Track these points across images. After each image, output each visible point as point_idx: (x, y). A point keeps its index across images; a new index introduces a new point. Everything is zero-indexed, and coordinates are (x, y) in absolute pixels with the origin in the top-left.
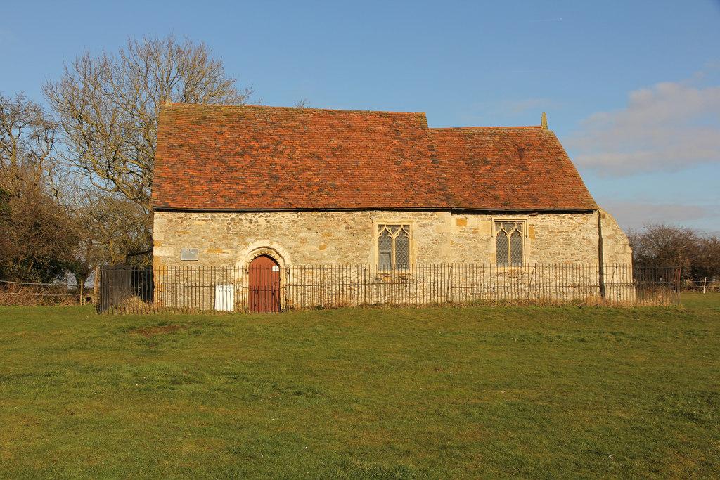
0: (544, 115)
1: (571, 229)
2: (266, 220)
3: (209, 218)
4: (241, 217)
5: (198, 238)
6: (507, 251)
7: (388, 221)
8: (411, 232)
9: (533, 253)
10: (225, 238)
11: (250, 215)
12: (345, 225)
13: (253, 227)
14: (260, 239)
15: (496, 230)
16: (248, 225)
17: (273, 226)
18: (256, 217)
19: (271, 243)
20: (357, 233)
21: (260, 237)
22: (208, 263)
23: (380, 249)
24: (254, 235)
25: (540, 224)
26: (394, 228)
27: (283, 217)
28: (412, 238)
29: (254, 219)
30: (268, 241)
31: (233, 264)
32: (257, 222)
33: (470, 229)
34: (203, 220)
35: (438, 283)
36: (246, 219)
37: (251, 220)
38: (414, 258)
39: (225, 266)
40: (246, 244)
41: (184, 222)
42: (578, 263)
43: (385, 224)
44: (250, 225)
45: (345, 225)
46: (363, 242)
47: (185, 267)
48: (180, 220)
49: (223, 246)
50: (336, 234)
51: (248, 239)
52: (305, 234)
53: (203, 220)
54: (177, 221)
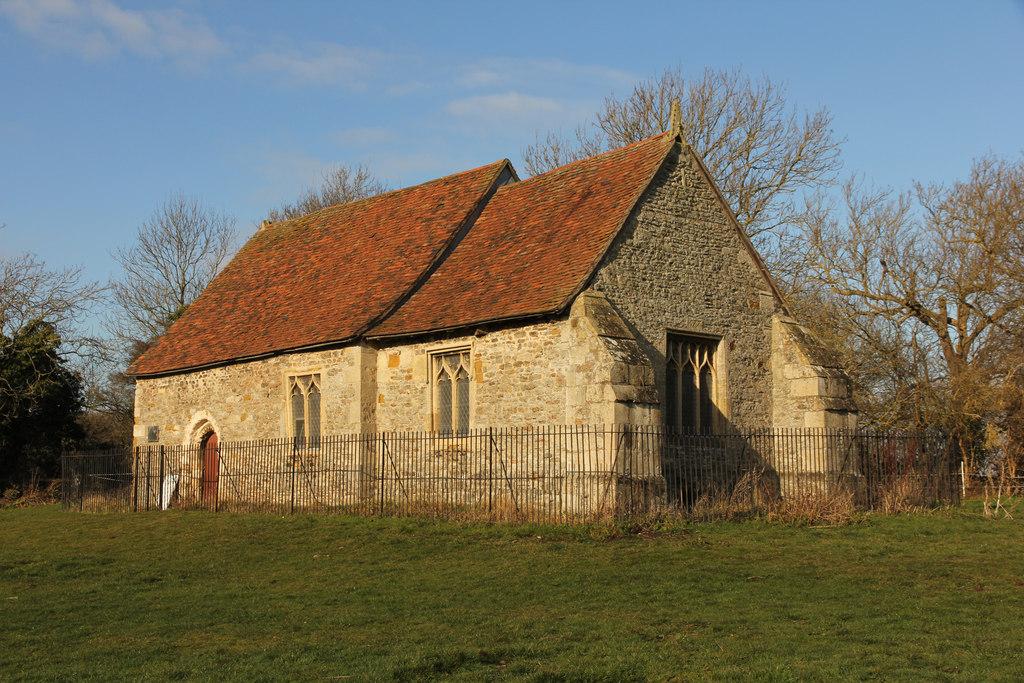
5: (160, 411)
7: (298, 369)
14: (199, 410)
25: (490, 351)
50: (256, 396)
51: (192, 411)
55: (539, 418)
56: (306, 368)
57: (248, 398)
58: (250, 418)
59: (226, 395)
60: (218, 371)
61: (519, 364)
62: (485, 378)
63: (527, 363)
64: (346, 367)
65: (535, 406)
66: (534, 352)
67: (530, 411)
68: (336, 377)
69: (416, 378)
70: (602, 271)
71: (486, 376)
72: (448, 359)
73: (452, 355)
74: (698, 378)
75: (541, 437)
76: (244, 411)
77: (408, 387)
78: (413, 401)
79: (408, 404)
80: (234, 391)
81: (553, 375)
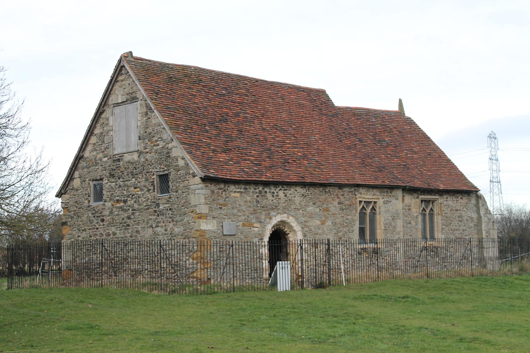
0: (400, 101)
1: (462, 207)
2: (284, 193)
3: (242, 190)
4: (266, 189)
5: (235, 211)
6: (370, 224)
7: (366, 197)
8: (378, 208)
9: (442, 229)
10: (255, 212)
11: (273, 189)
12: (338, 200)
13: (275, 201)
14: (280, 213)
15: (359, 206)
16: (271, 198)
17: (290, 200)
18: (277, 191)
19: (288, 218)
20: (346, 209)
21: (280, 211)
22: (243, 237)
23: (360, 224)
24: (275, 208)
25: (445, 203)
26: (368, 203)
27: (296, 190)
28: (380, 213)
29: (275, 192)
30: (286, 215)
31: (262, 239)
32: (277, 196)
33: (407, 206)
34: (238, 192)
35: (142, 245)
36: (270, 192)
37: (273, 193)
38: (380, 235)
39: (255, 240)
40: (271, 218)
41: (224, 193)
42: (467, 237)
43: (363, 200)
44: (273, 198)
45: (338, 200)
46: (349, 217)
47: (225, 241)
48: (220, 191)
49: (254, 221)
50: (332, 209)
51: (273, 213)
52: (310, 209)
53: (238, 192)
54: (218, 192)
55: (466, 234)
56: (371, 197)
57: (327, 210)
58: (329, 223)
59: (307, 206)
60: (299, 189)
61: (457, 210)
62: (444, 215)
63: (460, 210)
64: (394, 201)
65: (464, 229)
66: (462, 206)
67: (462, 231)
68: (389, 204)
69: (413, 210)
70: (120, 101)
71: (445, 213)
72: (426, 203)
73: (427, 202)
74: (368, 216)
75: (419, 243)
76: (323, 218)
77: (409, 214)
78: (412, 222)
79: (410, 223)
80: (314, 204)
81: (469, 217)
